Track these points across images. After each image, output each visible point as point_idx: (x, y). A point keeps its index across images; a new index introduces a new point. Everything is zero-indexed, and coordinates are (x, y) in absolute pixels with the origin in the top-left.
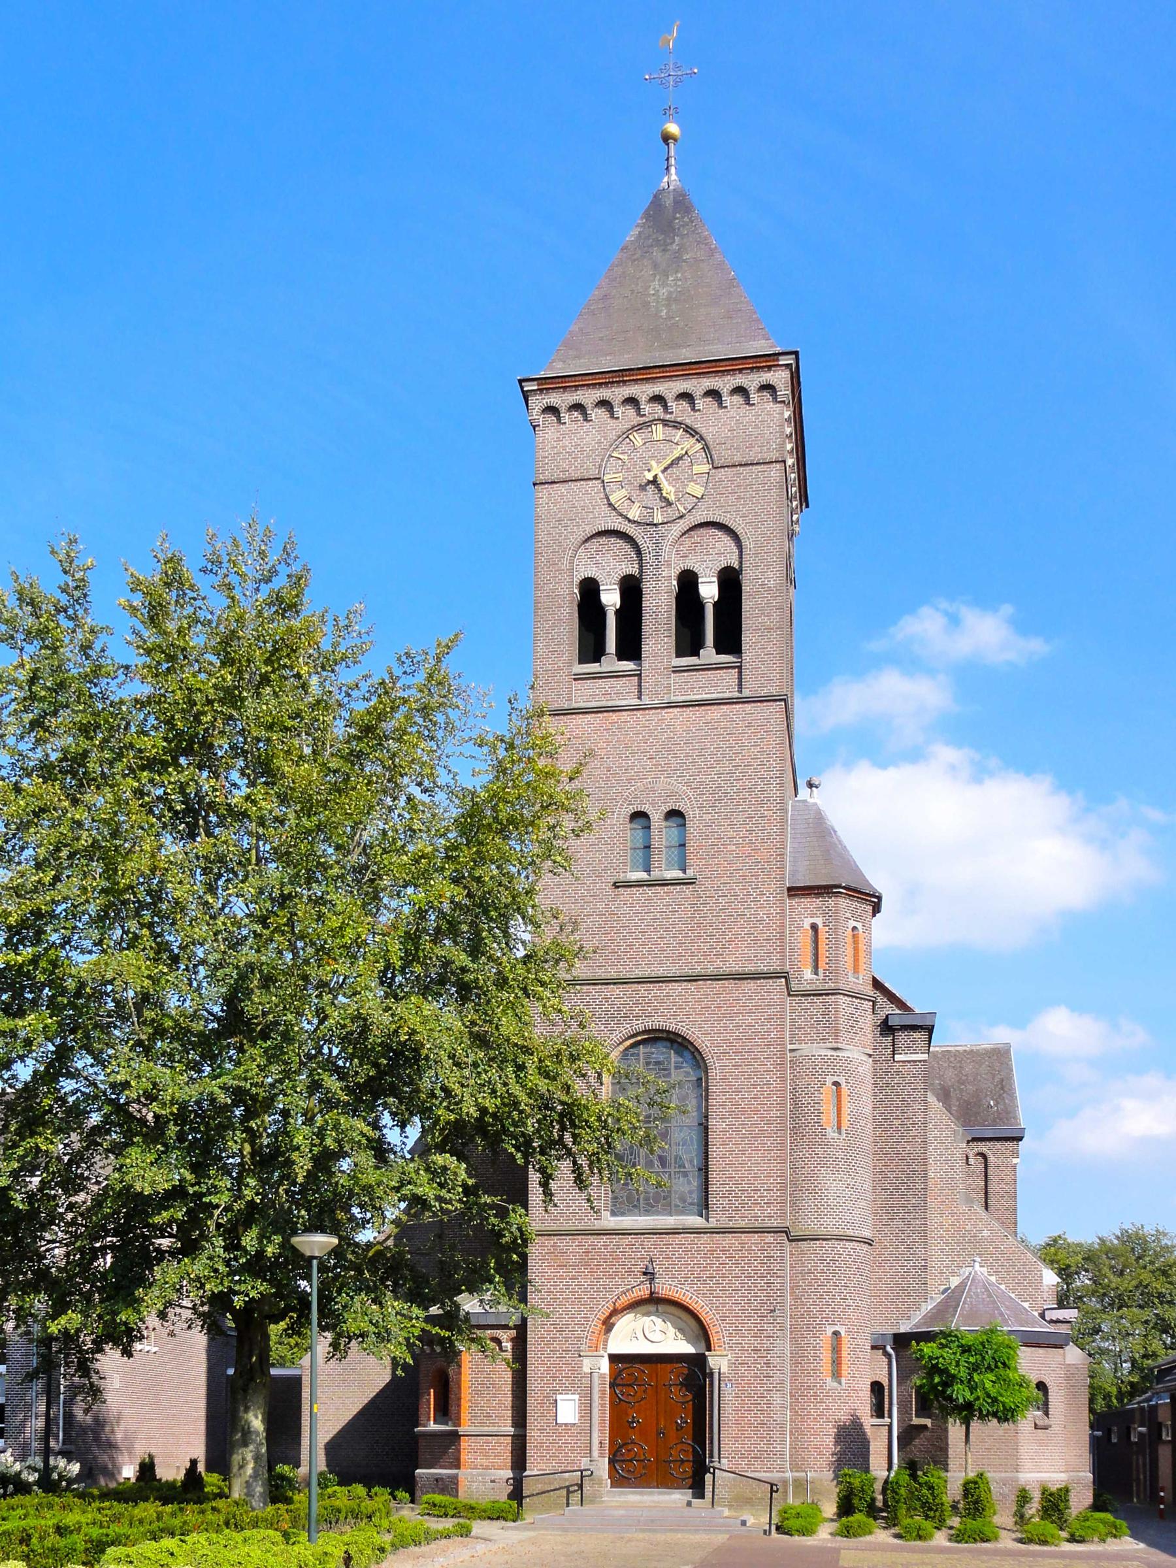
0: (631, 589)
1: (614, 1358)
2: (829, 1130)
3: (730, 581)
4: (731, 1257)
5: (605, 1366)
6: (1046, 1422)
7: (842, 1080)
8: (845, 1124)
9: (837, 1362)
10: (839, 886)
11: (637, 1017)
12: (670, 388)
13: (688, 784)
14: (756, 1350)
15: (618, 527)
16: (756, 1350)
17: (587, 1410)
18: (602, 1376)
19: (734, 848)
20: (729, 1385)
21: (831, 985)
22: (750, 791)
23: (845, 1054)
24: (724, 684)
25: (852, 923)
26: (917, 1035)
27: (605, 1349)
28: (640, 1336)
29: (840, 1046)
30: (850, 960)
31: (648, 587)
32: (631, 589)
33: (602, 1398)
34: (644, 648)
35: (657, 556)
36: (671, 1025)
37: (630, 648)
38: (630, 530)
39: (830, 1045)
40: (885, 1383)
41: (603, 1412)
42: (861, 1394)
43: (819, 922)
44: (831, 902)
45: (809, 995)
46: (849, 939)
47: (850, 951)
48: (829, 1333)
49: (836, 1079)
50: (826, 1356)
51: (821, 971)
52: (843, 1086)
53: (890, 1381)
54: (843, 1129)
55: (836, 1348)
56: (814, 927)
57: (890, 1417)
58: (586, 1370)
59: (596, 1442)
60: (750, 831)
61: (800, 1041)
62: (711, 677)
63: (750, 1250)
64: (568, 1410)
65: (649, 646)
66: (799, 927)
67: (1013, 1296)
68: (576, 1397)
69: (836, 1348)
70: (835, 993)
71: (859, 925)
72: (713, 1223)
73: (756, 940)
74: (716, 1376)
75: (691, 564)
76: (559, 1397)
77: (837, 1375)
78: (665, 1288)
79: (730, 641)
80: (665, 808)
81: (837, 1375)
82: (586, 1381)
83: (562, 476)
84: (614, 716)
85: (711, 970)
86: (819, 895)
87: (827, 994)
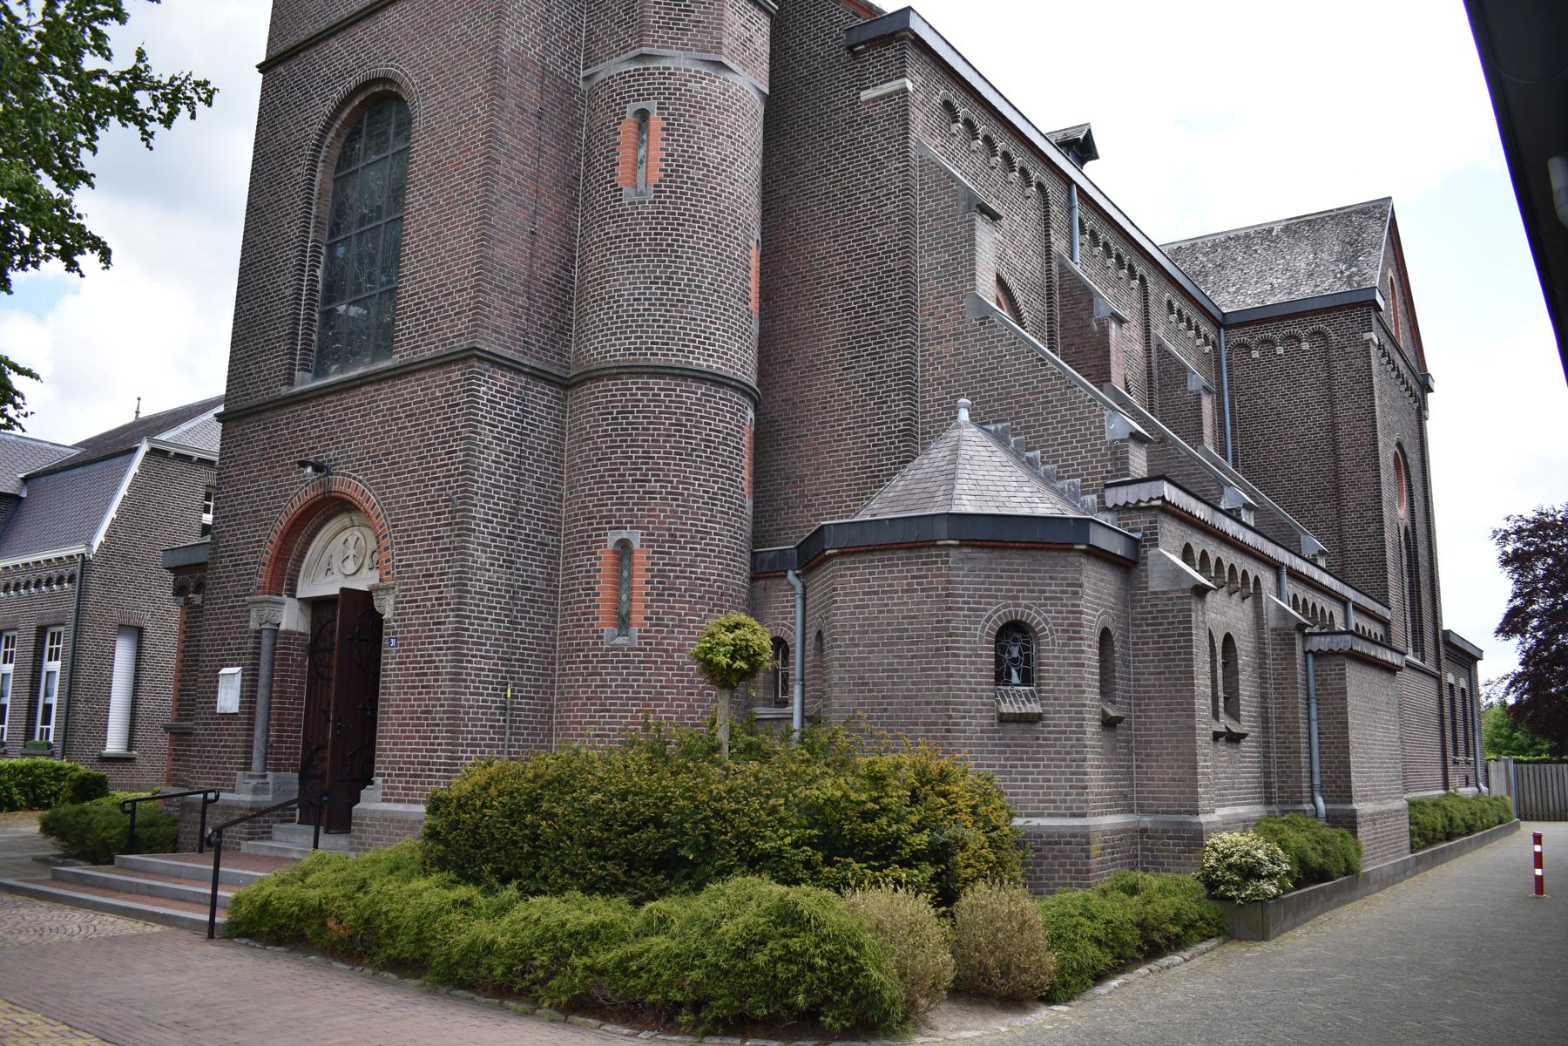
5: (291, 618)
27: (292, 593)
29: (645, 50)
48: (611, 544)
49: (642, 105)
82: (251, 644)
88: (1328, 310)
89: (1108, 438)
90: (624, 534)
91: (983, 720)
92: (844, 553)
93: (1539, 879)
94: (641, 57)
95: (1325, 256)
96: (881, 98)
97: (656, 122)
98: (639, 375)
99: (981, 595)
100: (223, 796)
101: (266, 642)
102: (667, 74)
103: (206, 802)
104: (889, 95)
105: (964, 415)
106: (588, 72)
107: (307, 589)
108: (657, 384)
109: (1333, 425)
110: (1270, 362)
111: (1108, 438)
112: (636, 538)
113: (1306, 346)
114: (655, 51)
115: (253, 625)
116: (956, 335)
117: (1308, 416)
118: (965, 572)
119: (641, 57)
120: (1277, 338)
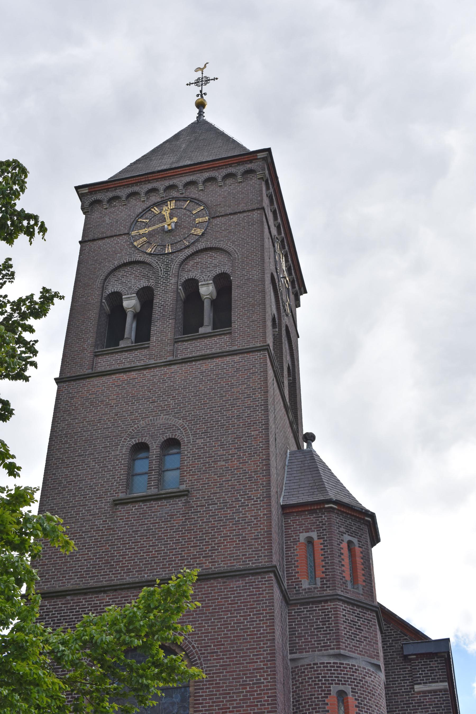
0: (146, 296)
3: (223, 283)
7: (348, 689)
10: (330, 501)
12: (180, 181)
13: (184, 418)
15: (141, 259)
21: (329, 592)
22: (239, 417)
23: (351, 662)
26: (433, 664)
29: (342, 652)
30: (347, 574)
32: (146, 296)
34: (154, 329)
35: (167, 272)
37: (143, 335)
38: (149, 259)
39: (331, 652)
43: (314, 535)
45: (308, 603)
46: (345, 551)
47: (346, 561)
49: (341, 687)
51: (318, 580)
52: (350, 695)
56: (310, 541)
60: (239, 449)
67: (292, 700)
70: (335, 598)
79: (223, 319)
80: (162, 439)
83: (101, 236)
86: (312, 512)
87: (326, 601)
96: (430, 692)
104: (435, 691)
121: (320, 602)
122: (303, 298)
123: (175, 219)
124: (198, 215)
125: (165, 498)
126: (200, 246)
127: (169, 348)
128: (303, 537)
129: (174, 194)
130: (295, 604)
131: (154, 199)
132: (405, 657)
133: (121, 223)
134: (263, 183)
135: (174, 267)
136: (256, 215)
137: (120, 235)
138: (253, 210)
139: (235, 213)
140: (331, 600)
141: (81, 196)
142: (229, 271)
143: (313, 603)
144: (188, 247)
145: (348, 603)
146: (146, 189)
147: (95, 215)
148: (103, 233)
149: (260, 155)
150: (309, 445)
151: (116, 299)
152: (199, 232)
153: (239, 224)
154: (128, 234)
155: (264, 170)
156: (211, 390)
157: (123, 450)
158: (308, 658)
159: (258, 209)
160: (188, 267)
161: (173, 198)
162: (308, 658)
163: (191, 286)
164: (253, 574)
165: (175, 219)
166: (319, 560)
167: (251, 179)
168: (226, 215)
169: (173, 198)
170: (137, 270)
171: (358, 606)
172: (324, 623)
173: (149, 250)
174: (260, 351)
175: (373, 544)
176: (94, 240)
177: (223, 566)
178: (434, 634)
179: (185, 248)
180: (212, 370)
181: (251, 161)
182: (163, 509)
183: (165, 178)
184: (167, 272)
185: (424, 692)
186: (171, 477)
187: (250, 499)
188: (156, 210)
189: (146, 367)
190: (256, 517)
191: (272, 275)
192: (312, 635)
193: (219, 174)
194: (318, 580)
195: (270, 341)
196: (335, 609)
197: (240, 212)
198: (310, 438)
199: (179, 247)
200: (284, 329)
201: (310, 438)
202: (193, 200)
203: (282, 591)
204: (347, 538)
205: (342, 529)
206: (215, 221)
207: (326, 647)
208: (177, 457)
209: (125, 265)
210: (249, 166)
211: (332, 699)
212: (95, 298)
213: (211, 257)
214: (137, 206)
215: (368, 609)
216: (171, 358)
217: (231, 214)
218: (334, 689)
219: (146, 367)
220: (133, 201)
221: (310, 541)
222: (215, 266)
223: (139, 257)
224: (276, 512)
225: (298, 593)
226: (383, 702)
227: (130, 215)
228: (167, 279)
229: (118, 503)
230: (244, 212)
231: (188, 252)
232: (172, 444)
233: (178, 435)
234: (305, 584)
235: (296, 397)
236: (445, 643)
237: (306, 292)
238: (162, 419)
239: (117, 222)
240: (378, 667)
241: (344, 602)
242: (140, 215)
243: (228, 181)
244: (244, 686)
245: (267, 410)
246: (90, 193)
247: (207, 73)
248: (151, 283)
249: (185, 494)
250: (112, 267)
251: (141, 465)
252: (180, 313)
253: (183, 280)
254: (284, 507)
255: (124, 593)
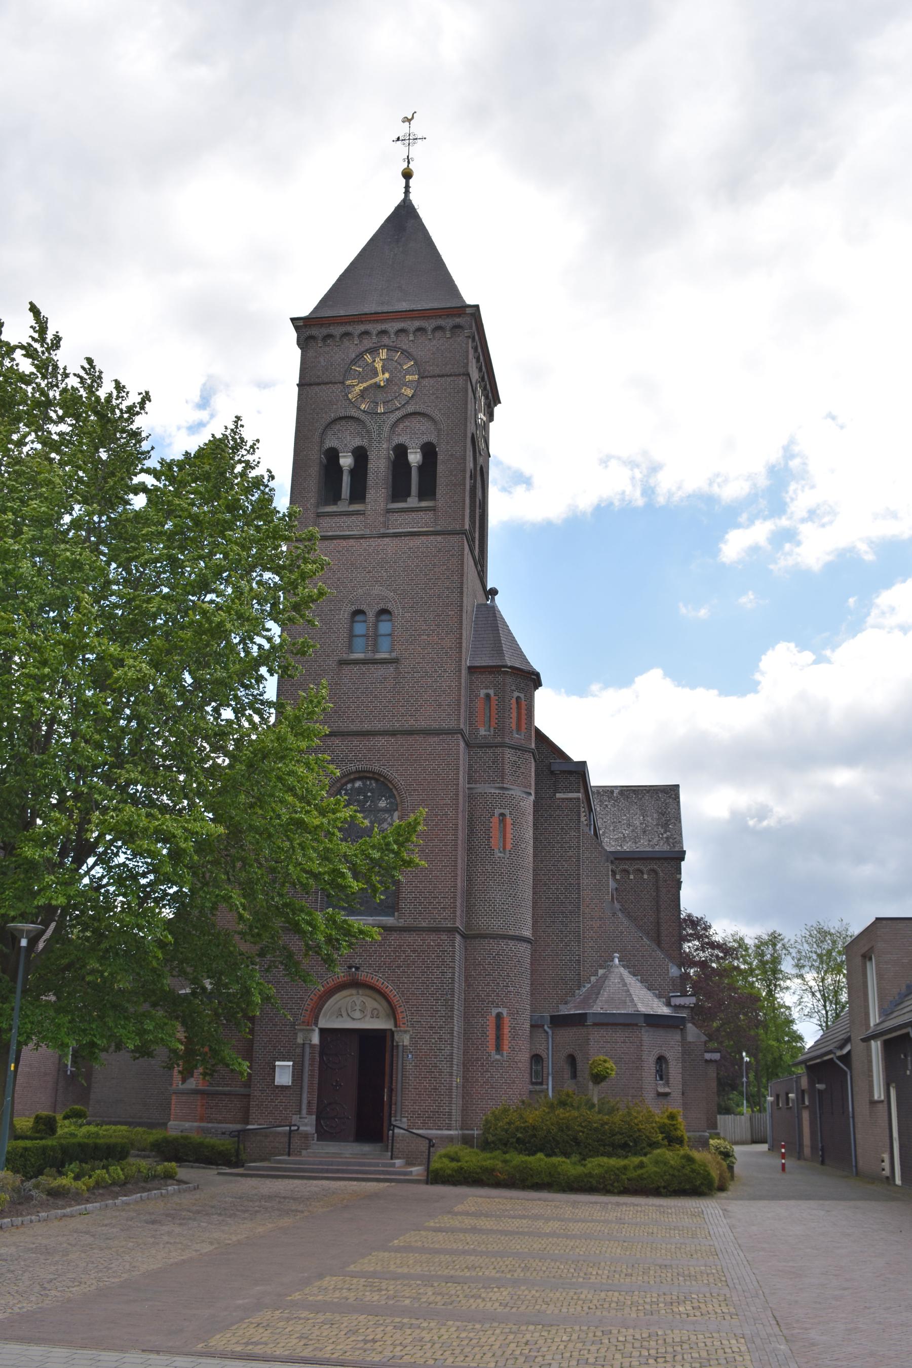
0: (361, 455)
1: (323, 1031)
2: (496, 851)
3: (429, 451)
4: (414, 951)
5: (316, 1039)
6: (667, 1090)
7: (507, 812)
8: (509, 846)
9: (499, 1038)
10: (506, 666)
11: (351, 761)
13: (395, 591)
14: (431, 1027)
15: (356, 415)
16: (431, 1027)
17: (297, 1074)
18: (312, 1046)
19: (426, 637)
20: (410, 1056)
21: (499, 739)
22: (439, 597)
24: (422, 522)
25: (516, 694)
26: (572, 779)
27: (316, 1024)
28: (344, 1014)
29: (505, 786)
30: (514, 721)
31: (372, 456)
32: (361, 455)
33: (311, 1065)
34: (368, 496)
35: (379, 434)
36: (376, 767)
37: (359, 494)
38: (363, 417)
39: (497, 785)
40: (544, 1055)
41: (311, 1076)
42: (520, 1065)
43: (491, 692)
44: (500, 678)
45: (483, 747)
46: (514, 706)
47: (514, 715)
48: (494, 1014)
49: (502, 811)
50: (491, 1033)
51: (492, 729)
52: (508, 817)
53: (548, 1055)
54: (507, 850)
55: (499, 1026)
56: (488, 696)
57: (548, 1085)
58: (300, 1041)
59: (305, 1102)
61: (476, 782)
62: (414, 515)
63: (429, 945)
64: (284, 1073)
65: (371, 495)
66: (477, 696)
68: (291, 1063)
69: (499, 1026)
70: (502, 745)
71: (522, 696)
72: (401, 923)
73: (440, 705)
74: (401, 1049)
75: (402, 439)
76: (277, 1063)
77: (499, 1048)
78: (362, 976)
79: (428, 490)
80: (377, 608)
81: (499, 1048)
82: (298, 1050)
84: (344, 543)
85: (407, 726)
86: (491, 673)
87: (496, 747)
88: (659, 859)
89: (670, 975)
90: (500, 1010)
91: (652, 1095)
92: (595, 1024)
93: (783, 1165)
94: (503, 788)
95: (649, 819)
96: (567, 799)
97: (509, 820)
98: (505, 938)
99: (653, 1044)
100: (301, 1128)
101: (307, 1050)
102: (512, 797)
103: (291, 1131)
104: (571, 799)
105: (616, 961)
106: (471, 786)
107: (324, 1023)
108: (511, 943)
109: (658, 922)
110: (626, 882)
111: (670, 975)
112: (505, 1012)
113: (646, 877)
114: (511, 787)
115: (300, 1041)
116: (601, 919)
117: (645, 916)
118: (647, 1036)
119: (503, 788)
120: (631, 869)
121: (492, 747)
122: (497, 410)
123: (387, 375)
124: (408, 372)
125: (380, 663)
126: (410, 409)
127: (381, 519)
128: (483, 693)
129: (385, 340)
130: (474, 747)
131: (367, 343)
132: (552, 773)
133: (336, 368)
134: (470, 341)
135: (386, 428)
136: (461, 381)
137: (336, 383)
138: (459, 375)
139: (443, 376)
140: (501, 747)
141: (297, 328)
142: (435, 442)
143: (487, 747)
144: (398, 409)
145: (513, 748)
146: (359, 332)
147: (311, 353)
148: (318, 377)
149: (468, 311)
150: (493, 599)
151: (333, 455)
152: (409, 392)
153: (445, 389)
154: (343, 383)
155: (471, 328)
156: (417, 566)
157: (344, 614)
158: (481, 788)
159: (464, 374)
160: (398, 430)
161: (385, 346)
162: (481, 788)
163: (401, 451)
164: (445, 734)
165: (387, 375)
166: (494, 712)
167: (459, 336)
168: (434, 376)
169: (385, 346)
170: (352, 426)
171: (519, 750)
172: (493, 763)
173: (363, 407)
174: (458, 534)
175: (536, 688)
176: (311, 385)
177: (423, 724)
178: (576, 757)
179: (396, 410)
180: (418, 548)
181: (459, 315)
182: (380, 672)
183: (377, 321)
184: (379, 434)
185: (563, 799)
186: (385, 644)
187: (445, 671)
188: (368, 358)
189: (362, 537)
190: (450, 687)
191: (473, 435)
192: (484, 771)
193: (429, 325)
194: (492, 729)
195: (467, 527)
196: (503, 753)
197: (447, 376)
198: (494, 592)
199: (391, 406)
200: (478, 469)
201: (494, 592)
202: (404, 352)
203: (465, 741)
204: (516, 694)
205: (513, 688)
206: (425, 382)
207: (494, 781)
208: (389, 624)
209: (341, 418)
210: (458, 320)
211: (495, 820)
212: (316, 457)
213: (419, 422)
214: (351, 349)
215: (526, 751)
216: (382, 531)
217: (439, 376)
218: (497, 812)
219: (362, 537)
220: (346, 343)
221: (488, 696)
222: (423, 434)
223: (353, 412)
224: (464, 672)
225: (476, 738)
226: (531, 818)
227: (343, 360)
228: (379, 443)
229: (342, 663)
230: (451, 375)
231: (399, 414)
232: (384, 612)
233: (389, 606)
234: (482, 732)
235: (483, 559)
236: (584, 764)
237: (500, 402)
238: (377, 590)
239: (332, 365)
240: (530, 794)
241: (509, 747)
242: (354, 362)
243: (438, 334)
244: (436, 815)
245: (462, 593)
246: (305, 326)
247: (416, 128)
248: (365, 443)
249: (395, 661)
250: (329, 420)
251: (360, 629)
252: (390, 477)
253: (394, 444)
254: (470, 668)
255: (350, 738)
